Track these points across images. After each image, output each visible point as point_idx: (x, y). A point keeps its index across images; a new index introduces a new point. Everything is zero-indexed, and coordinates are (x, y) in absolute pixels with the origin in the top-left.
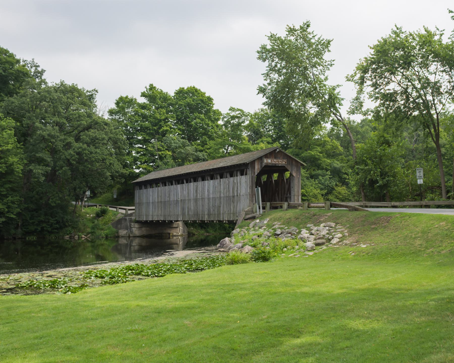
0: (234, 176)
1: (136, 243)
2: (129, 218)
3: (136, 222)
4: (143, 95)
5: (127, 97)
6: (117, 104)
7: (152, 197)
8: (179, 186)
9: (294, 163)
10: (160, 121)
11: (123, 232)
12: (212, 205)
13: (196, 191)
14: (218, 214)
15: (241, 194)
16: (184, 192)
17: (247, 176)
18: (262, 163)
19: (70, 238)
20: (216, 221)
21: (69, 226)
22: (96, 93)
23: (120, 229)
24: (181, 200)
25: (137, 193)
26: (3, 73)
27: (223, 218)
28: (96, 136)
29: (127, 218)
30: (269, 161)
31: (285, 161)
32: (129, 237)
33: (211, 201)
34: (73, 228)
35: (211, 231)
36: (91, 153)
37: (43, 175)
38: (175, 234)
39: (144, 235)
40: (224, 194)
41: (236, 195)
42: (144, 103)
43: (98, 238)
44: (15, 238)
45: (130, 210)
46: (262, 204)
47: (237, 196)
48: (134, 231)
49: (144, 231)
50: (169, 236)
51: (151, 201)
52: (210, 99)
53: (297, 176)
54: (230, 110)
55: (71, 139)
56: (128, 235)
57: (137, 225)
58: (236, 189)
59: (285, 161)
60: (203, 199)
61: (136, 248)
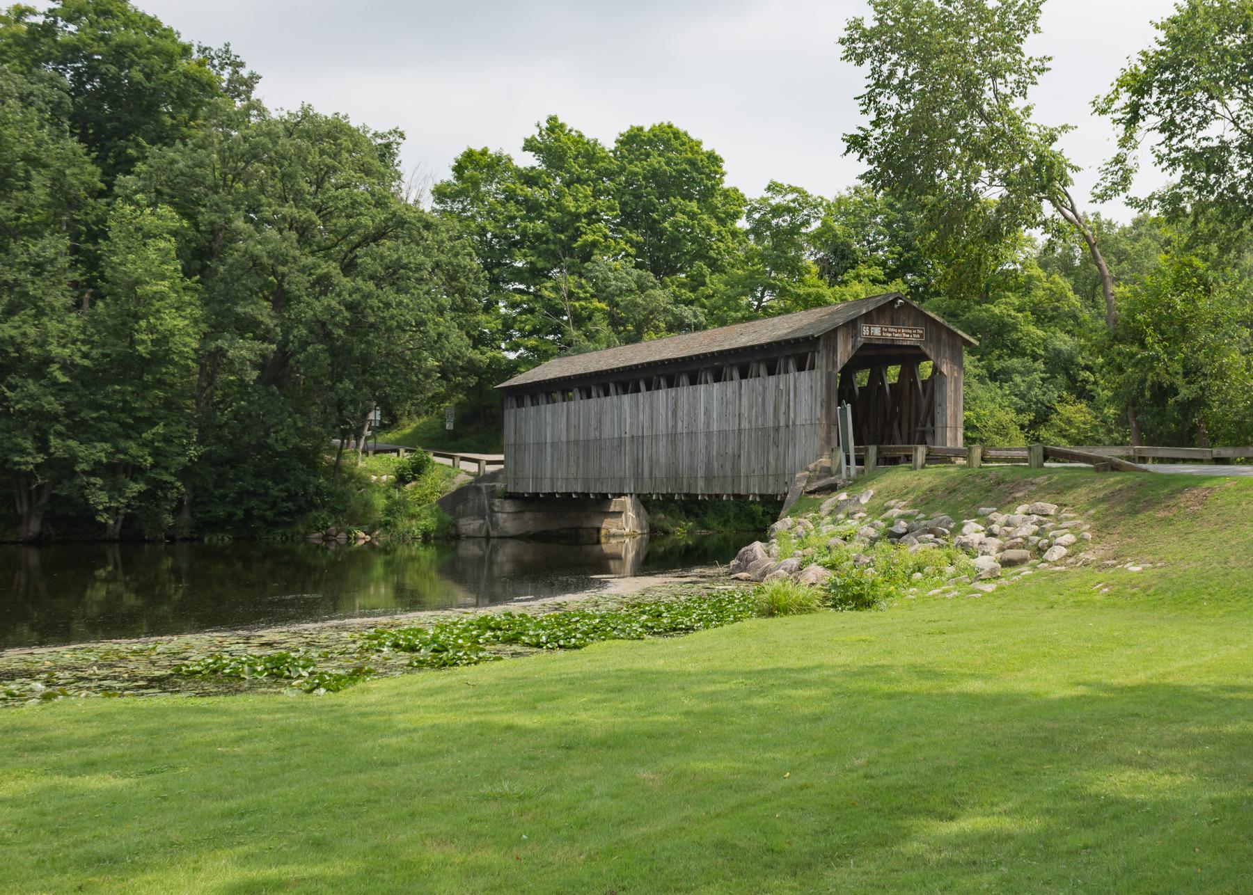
0: (779, 373)
2: (486, 487)
3: (506, 498)
4: (530, 146)
5: (484, 153)
6: (459, 169)
8: (626, 399)
9: (944, 336)
11: (470, 525)
12: (718, 453)
13: (675, 413)
15: (798, 423)
17: (813, 372)
18: (855, 336)
19: (326, 538)
20: (728, 495)
22: (401, 140)
24: (633, 437)
25: (511, 416)
27: (748, 488)
28: (400, 258)
29: (483, 485)
31: (921, 332)
32: (488, 538)
34: (334, 511)
36: (388, 305)
37: (255, 366)
38: (613, 530)
39: (529, 532)
40: (750, 422)
41: (782, 423)
42: (533, 168)
43: (403, 539)
44: (172, 539)
45: (489, 463)
46: (856, 450)
47: (787, 426)
48: (501, 522)
49: (530, 522)
52: (714, 159)
53: (952, 373)
54: (769, 189)
56: (483, 533)
57: (509, 506)
58: (783, 410)
59: (921, 332)
60: (692, 434)
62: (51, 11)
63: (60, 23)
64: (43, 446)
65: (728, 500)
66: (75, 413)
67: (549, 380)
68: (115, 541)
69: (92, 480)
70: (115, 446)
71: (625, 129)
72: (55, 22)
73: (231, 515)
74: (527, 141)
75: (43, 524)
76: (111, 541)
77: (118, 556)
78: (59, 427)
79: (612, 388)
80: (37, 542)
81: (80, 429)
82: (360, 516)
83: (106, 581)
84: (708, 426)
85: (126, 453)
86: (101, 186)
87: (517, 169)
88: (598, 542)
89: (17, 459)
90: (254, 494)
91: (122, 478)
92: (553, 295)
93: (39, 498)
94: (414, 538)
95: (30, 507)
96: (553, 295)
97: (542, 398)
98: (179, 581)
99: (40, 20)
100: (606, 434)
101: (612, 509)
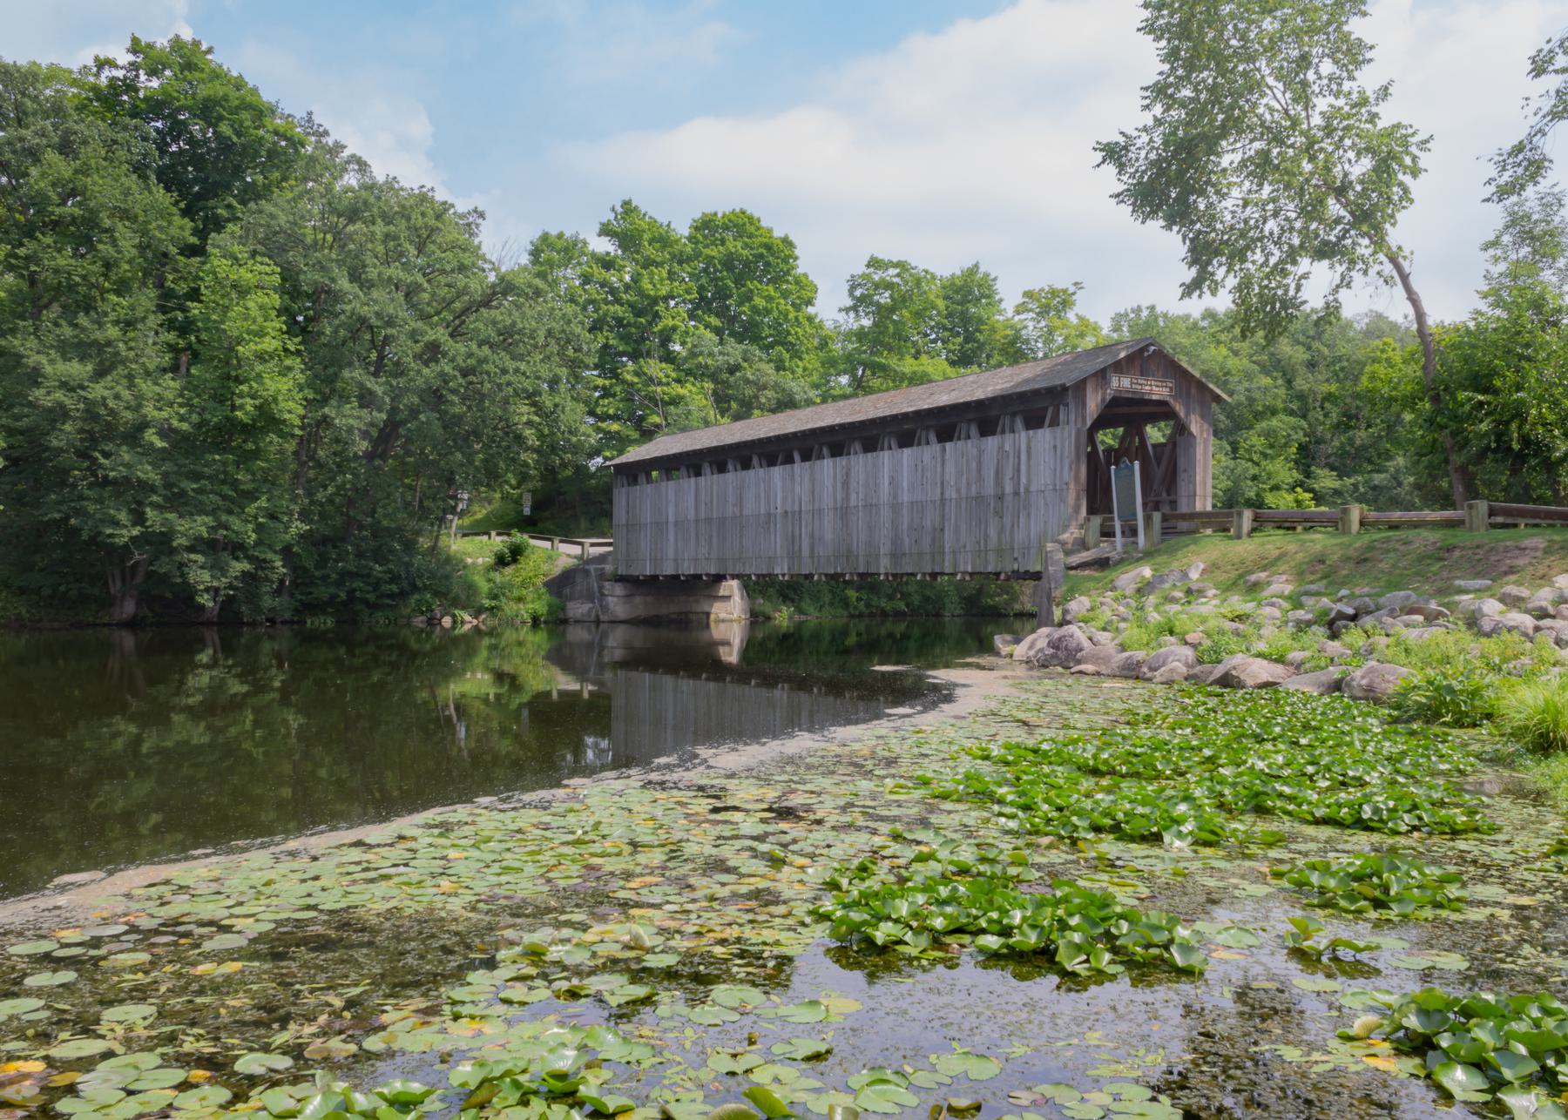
0: (1003, 432)
1: (616, 642)
4: (605, 231)
5: (560, 236)
6: (535, 253)
7: (677, 506)
8: (777, 472)
9: (1193, 391)
10: (654, 301)
11: (578, 609)
13: (846, 484)
14: (933, 555)
15: (1033, 488)
16: (797, 488)
17: (1058, 430)
20: (924, 575)
21: (426, 588)
22: (480, 221)
23: (572, 598)
25: (621, 496)
26: (235, 139)
27: (955, 566)
28: (514, 324)
29: (592, 568)
30: (1122, 383)
32: (598, 622)
33: (905, 511)
34: (436, 594)
35: (811, 610)
36: (504, 371)
37: (365, 435)
38: (722, 615)
40: (958, 491)
41: (1008, 489)
42: (608, 254)
43: (511, 623)
44: (272, 621)
45: (593, 545)
47: (1016, 493)
48: (611, 606)
49: (640, 606)
50: (704, 621)
51: (671, 519)
52: (786, 242)
54: (868, 266)
55: (440, 334)
56: (593, 618)
57: (619, 589)
58: (1009, 473)
60: (871, 508)
61: (618, 654)
62: (132, 64)
63: (143, 77)
64: (139, 519)
65: (963, 580)
66: (173, 485)
67: (674, 455)
68: (214, 624)
69: (192, 556)
70: (217, 519)
71: (698, 215)
72: (137, 76)
73: (333, 597)
74: (603, 224)
75: (138, 604)
76: (209, 624)
77: (217, 641)
78: (155, 498)
79: (755, 461)
80: (132, 624)
81: (177, 501)
82: (465, 598)
83: (208, 667)
84: (895, 497)
85: (226, 528)
86: (194, 240)
87: (594, 255)
88: (708, 626)
89: (109, 531)
90: (353, 575)
91: (225, 556)
92: (636, 380)
93: (133, 577)
94: (524, 622)
95: (124, 583)
96: (636, 380)
97: (642, 478)
98: (280, 666)
99: (120, 74)
100: (749, 508)
101: (722, 593)
